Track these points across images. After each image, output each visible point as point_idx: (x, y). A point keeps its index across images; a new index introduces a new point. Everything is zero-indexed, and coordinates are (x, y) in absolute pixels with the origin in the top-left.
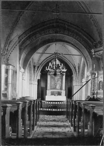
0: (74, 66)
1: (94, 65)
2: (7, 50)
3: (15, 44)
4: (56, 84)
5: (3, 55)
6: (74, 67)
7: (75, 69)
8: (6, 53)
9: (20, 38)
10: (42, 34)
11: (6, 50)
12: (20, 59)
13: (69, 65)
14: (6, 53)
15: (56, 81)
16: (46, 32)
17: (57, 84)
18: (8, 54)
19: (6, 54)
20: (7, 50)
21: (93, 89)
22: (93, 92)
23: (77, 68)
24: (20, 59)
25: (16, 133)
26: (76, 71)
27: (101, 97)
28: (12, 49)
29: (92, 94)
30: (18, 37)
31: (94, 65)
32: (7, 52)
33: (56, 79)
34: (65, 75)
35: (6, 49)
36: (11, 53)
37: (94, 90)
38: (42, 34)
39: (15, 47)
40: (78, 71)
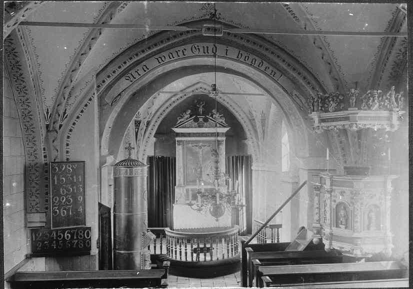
0: (251, 118)
1: (328, 150)
2: (65, 113)
3: (81, 102)
4: (199, 170)
5: (51, 129)
6: (250, 120)
7: (254, 126)
8: (59, 123)
9: (103, 76)
10: (163, 59)
11: (59, 115)
12: (101, 135)
13: (236, 114)
14: (59, 123)
15: (201, 159)
16: (175, 55)
17: (203, 170)
18: (67, 124)
19: (61, 126)
20: (65, 113)
21: (316, 217)
22: (318, 225)
23: (258, 125)
24: (101, 135)
25: (99, 270)
26: (256, 131)
27: (343, 250)
28: (75, 118)
29: (315, 232)
30: (94, 74)
31: (328, 150)
32: (62, 120)
33: (200, 155)
34: (224, 142)
35: (61, 113)
36: (86, 105)
37: (319, 221)
38: (163, 59)
39: (86, 105)
40: (262, 132)
